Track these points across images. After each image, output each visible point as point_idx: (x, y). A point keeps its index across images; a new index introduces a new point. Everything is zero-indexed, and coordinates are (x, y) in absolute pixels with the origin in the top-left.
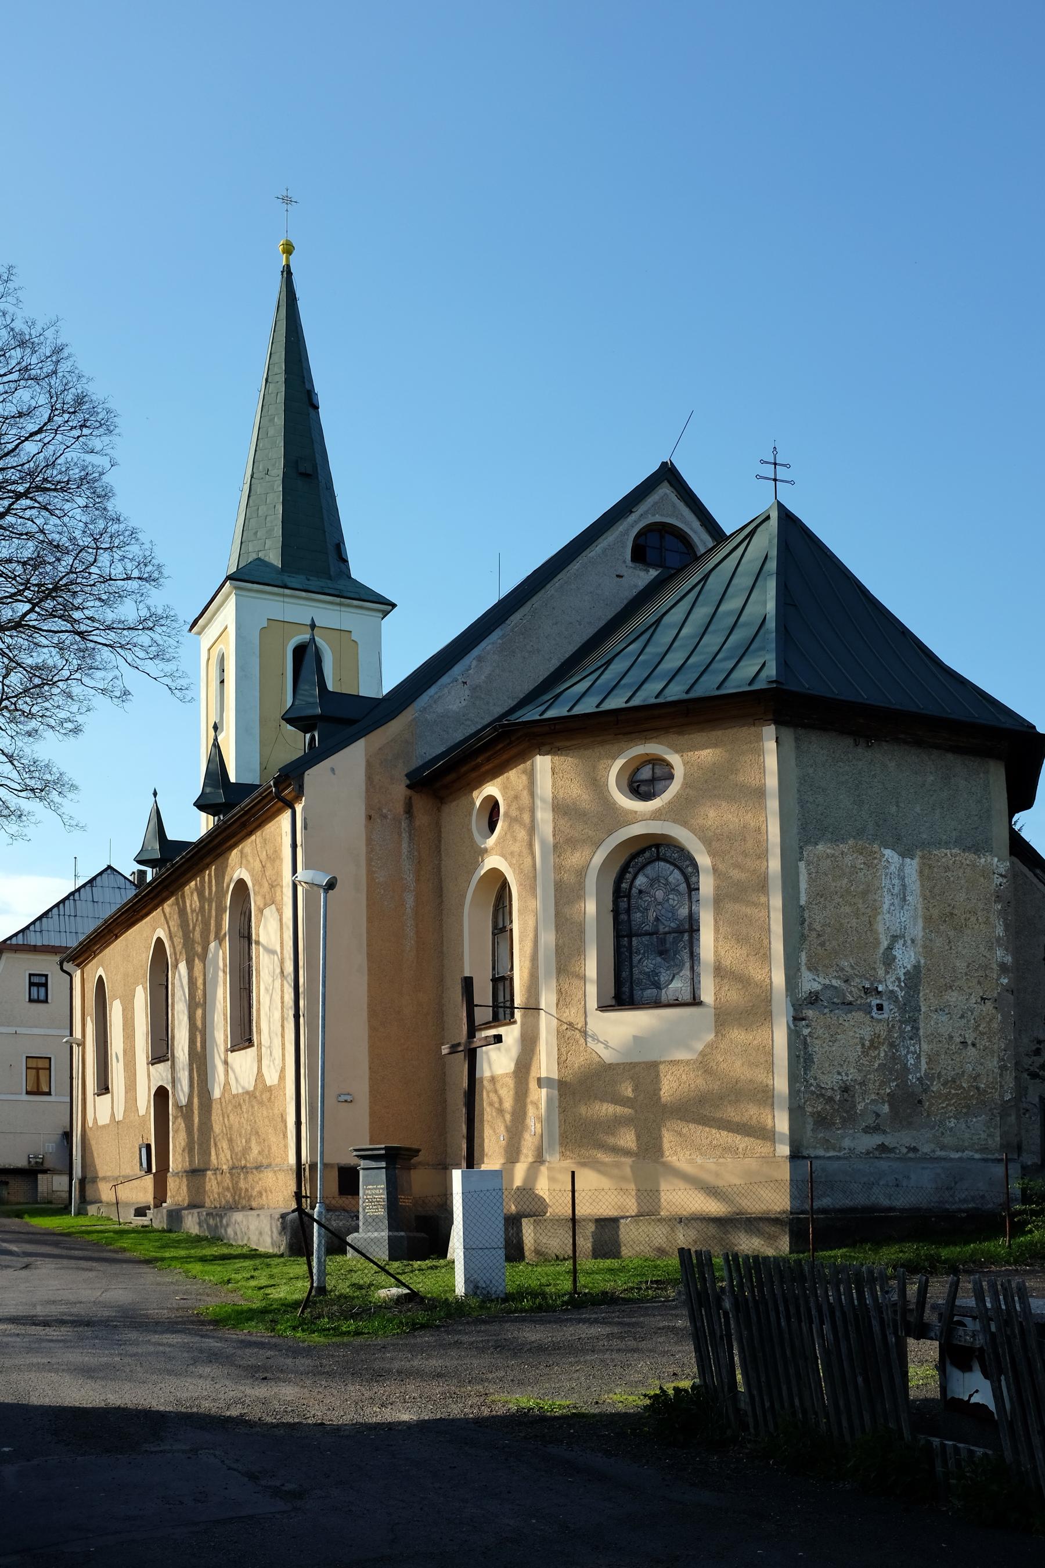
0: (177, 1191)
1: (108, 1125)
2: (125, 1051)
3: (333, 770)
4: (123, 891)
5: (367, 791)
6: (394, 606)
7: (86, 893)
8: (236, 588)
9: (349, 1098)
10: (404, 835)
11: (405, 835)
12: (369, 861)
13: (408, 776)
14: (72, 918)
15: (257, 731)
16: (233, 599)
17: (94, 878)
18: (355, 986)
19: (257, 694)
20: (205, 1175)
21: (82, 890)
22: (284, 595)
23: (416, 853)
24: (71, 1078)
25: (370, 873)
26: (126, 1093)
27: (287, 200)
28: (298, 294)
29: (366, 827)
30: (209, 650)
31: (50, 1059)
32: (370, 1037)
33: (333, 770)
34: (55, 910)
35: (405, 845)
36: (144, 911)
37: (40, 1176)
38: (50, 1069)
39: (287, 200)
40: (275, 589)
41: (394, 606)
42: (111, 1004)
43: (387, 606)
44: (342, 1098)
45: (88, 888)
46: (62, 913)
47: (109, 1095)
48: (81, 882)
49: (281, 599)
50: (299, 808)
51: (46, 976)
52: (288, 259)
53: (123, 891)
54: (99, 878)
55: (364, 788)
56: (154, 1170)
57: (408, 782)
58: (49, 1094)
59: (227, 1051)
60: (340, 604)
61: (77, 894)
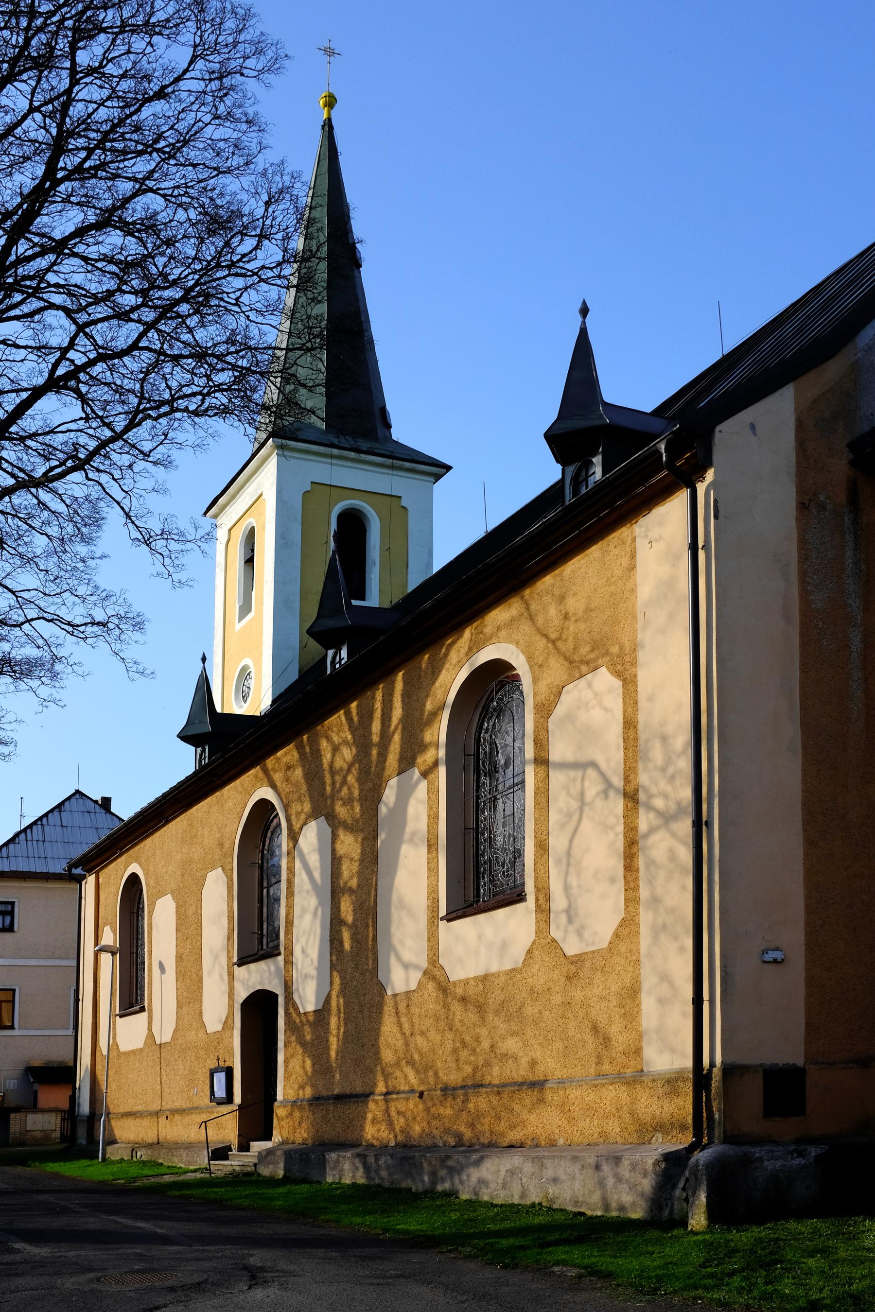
0: (288, 1128)
1: (141, 1050)
2: (179, 958)
3: (753, 427)
4: (92, 815)
5: (798, 462)
6: (448, 468)
7: (54, 818)
8: (280, 447)
9: (778, 955)
10: (848, 537)
11: (849, 537)
12: (803, 575)
13: (849, 445)
14: (41, 843)
15: (297, 605)
16: (273, 461)
17: (62, 803)
18: (784, 773)
19: (299, 564)
20: (366, 1103)
21: (50, 815)
22: (332, 456)
23: (863, 567)
24: (77, 1000)
25: (805, 595)
26: (179, 1006)
27: (330, 52)
28: (339, 149)
29: (798, 520)
30: (230, 530)
31: (14, 990)
32: (806, 856)
33: (753, 427)
34: (22, 836)
35: (849, 553)
36: (232, 772)
37: (12, 1116)
38: (13, 1001)
39: (330, 52)
40: (322, 449)
41: (448, 468)
42: (153, 905)
43: (439, 469)
44: (771, 956)
45: (56, 813)
46: (29, 838)
47: (143, 1016)
48: (27, 822)
49: (329, 461)
50: (701, 488)
51: (13, 904)
52: (329, 113)
53: (92, 815)
54: (67, 803)
55: (794, 460)
56: (238, 1099)
57: (851, 456)
58: (12, 1027)
59: (433, 919)
60: (392, 467)
61: (45, 820)
